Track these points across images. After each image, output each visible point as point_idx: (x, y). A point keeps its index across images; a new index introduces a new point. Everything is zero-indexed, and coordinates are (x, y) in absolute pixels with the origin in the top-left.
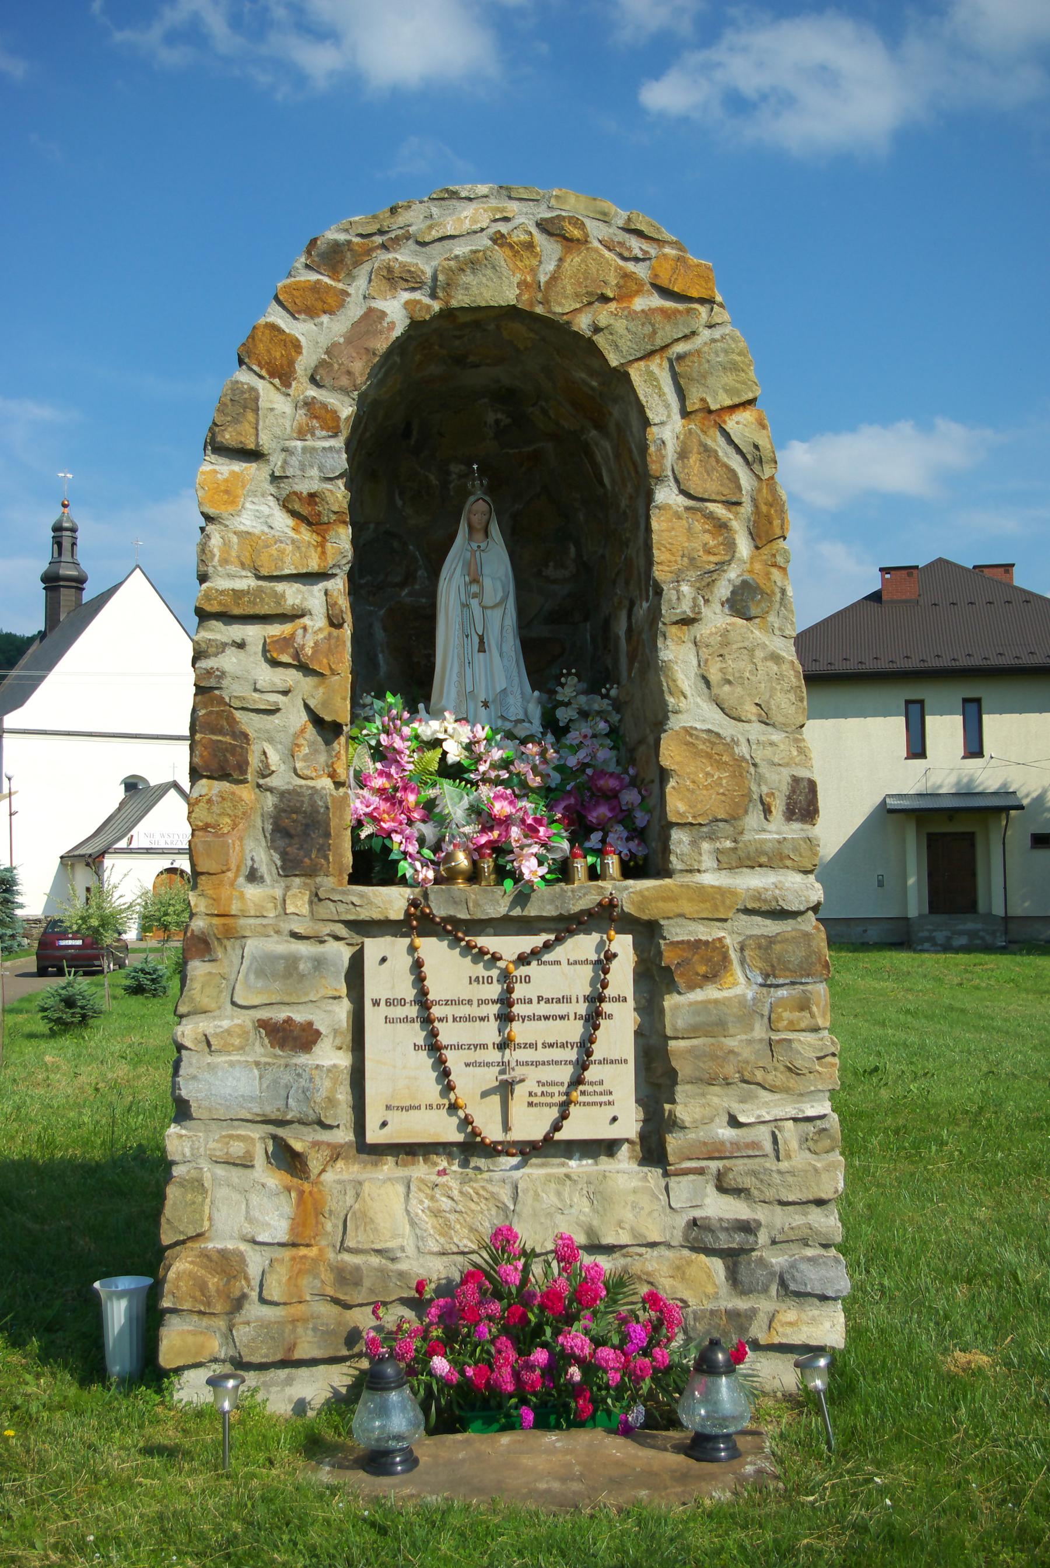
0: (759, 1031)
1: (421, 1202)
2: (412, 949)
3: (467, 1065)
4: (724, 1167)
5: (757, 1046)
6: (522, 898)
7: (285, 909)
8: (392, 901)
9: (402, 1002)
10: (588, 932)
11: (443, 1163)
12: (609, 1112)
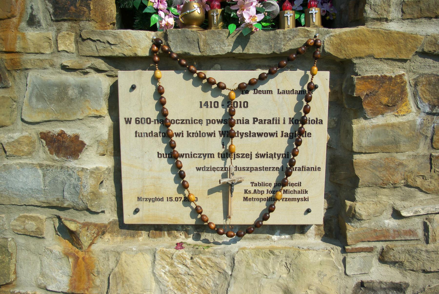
0: (423, 149)
1: (164, 267)
2: (155, 80)
3: (198, 169)
4: (387, 247)
5: (421, 160)
6: (243, 39)
7: (57, 47)
8: (140, 41)
9: (148, 121)
10: (293, 68)
11: (181, 237)
12: (305, 205)
